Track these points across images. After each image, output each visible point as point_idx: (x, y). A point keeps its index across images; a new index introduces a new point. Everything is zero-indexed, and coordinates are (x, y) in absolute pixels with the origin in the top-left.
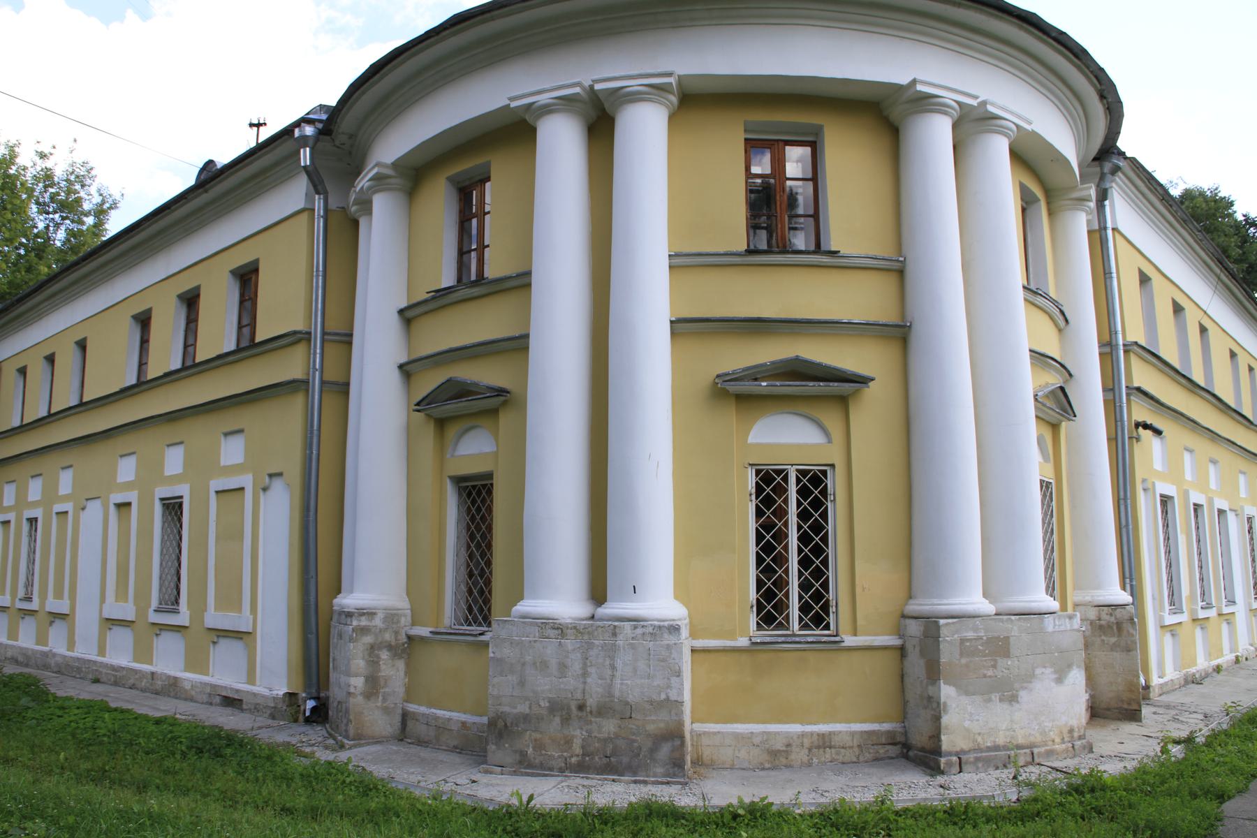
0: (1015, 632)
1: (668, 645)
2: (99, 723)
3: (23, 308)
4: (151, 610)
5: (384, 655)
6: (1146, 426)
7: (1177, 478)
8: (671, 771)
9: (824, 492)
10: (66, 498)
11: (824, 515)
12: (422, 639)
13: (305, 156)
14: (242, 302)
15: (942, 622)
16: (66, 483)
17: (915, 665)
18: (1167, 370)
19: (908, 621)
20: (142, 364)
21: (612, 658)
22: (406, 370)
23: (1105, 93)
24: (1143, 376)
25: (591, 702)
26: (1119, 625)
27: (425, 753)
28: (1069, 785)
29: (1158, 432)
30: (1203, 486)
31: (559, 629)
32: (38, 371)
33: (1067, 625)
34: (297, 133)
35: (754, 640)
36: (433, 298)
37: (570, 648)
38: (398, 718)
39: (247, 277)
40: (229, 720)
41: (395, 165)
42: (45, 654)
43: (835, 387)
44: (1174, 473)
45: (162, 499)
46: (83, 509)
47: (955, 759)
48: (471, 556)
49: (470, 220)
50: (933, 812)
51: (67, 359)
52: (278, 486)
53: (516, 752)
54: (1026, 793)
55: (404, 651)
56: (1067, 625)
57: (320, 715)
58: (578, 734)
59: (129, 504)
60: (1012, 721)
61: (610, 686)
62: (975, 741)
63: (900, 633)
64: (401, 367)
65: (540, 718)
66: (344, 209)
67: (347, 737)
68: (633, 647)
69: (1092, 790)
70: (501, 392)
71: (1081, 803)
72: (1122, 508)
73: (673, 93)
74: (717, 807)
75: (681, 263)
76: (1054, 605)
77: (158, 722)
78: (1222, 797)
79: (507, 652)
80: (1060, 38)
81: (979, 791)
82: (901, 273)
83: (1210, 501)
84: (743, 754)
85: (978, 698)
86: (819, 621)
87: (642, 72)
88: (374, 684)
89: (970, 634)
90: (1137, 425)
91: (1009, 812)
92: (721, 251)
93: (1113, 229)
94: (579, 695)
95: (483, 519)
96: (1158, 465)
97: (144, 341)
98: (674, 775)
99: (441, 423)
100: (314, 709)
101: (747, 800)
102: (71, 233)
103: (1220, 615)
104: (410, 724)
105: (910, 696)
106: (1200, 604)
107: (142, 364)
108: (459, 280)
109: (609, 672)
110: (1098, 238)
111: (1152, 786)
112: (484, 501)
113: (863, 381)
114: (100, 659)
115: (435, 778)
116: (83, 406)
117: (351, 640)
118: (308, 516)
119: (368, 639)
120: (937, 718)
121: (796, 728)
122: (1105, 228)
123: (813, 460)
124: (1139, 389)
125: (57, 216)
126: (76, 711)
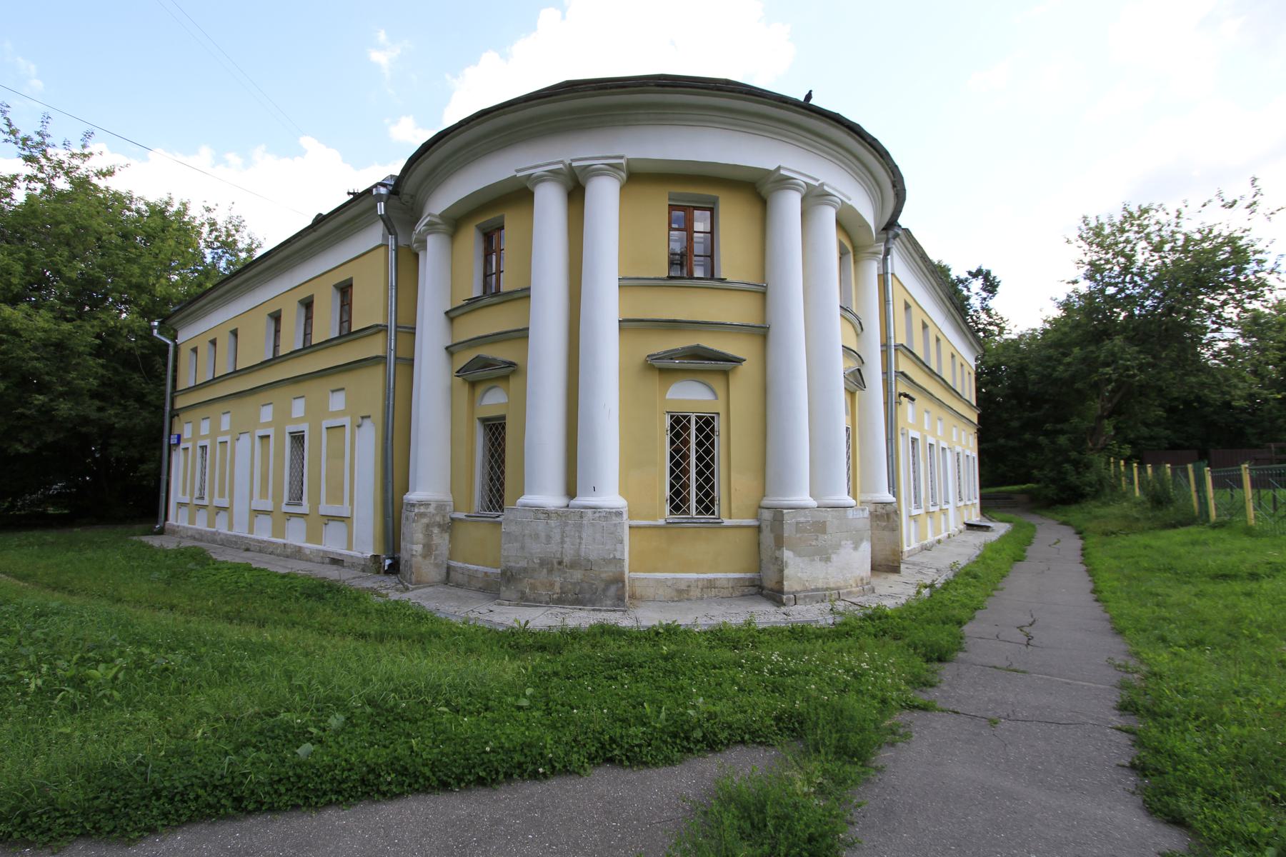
0: (829, 519)
1: (615, 524)
2: (242, 579)
3: (193, 308)
4: (283, 504)
5: (436, 530)
6: (906, 396)
7: (920, 429)
8: (616, 603)
9: (713, 430)
10: (226, 433)
11: (712, 444)
12: (460, 520)
13: (381, 208)
14: (342, 306)
15: (785, 511)
16: (226, 423)
17: (767, 537)
18: (918, 362)
19: (763, 510)
20: (276, 346)
21: (580, 532)
22: (451, 350)
23: (896, 184)
24: (905, 365)
25: (566, 560)
26: (888, 515)
27: (460, 592)
28: (865, 614)
29: (913, 399)
30: (934, 435)
31: (547, 513)
32: (204, 349)
33: (861, 514)
34: (374, 192)
35: (668, 521)
36: (468, 304)
37: (553, 525)
38: (444, 571)
39: (345, 290)
40: (332, 573)
41: (441, 216)
42: (214, 533)
43: (721, 365)
44: (918, 425)
45: (290, 433)
46: (238, 440)
47: (792, 596)
48: (492, 468)
49: (491, 254)
50: (782, 631)
51: (225, 342)
52: (367, 422)
53: (518, 591)
54: (838, 620)
55: (448, 528)
56: (861, 514)
57: (394, 569)
58: (558, 580)
59: (268, 436)
60: (827, 573)
61: (579, 549)
62: (804, 585)
63: (757, 517)
64: (447, 348)
65: (534, 570)
66: (409, 247)
67: (411, 583)
68: (593, 525)
69: (880, 618)
70: (511, 364)
71: (873, 626)
72: (889, 445)
73: (622, 170)
74: (646, 627)
75: (627, 284)
76: (853, 502)
77: (283, 576)
78: (960, 623)
79: (513, 528)
80: (873, 143)
81: (809, 617)
82: (764, 294)
83: (938, 442)
84: (661, 592)
85: (806, 559)
86: (708, 509)
87: (604, 155)
88: (428, 549)
89: (802, 519)
90: (900, 395)
91: (829, 632)
92: (652, 277)
93: (892, 274)
94: (558, 555)
95: (499, 445)
96: (910, 420)
97: (277, 331)
98: (619, 606)
99: (473, 385)
100: (390, 566)
101: (664, 623)
102: (229, 263)
103: (941, 510)
104: (452, 574)
105: (764, 557)
106: (931, 503)
107: (276, 346)
108: (485, 292)
109: (578, 541)
110: (883, 278)
111: (916, 615)
112: (500, 434)
113: (738, 361)
114: (250, 536)
115: (466, 610)
116: (236, 373)
117: (414, 521)
118: (387, 443)
119: (425, 521)
120: (781, 571)
121: (694, 576)
122: (887, 273)
123: (706, 410)
124: (902, 373)
125: (220, 251)
126: (227, 571)
